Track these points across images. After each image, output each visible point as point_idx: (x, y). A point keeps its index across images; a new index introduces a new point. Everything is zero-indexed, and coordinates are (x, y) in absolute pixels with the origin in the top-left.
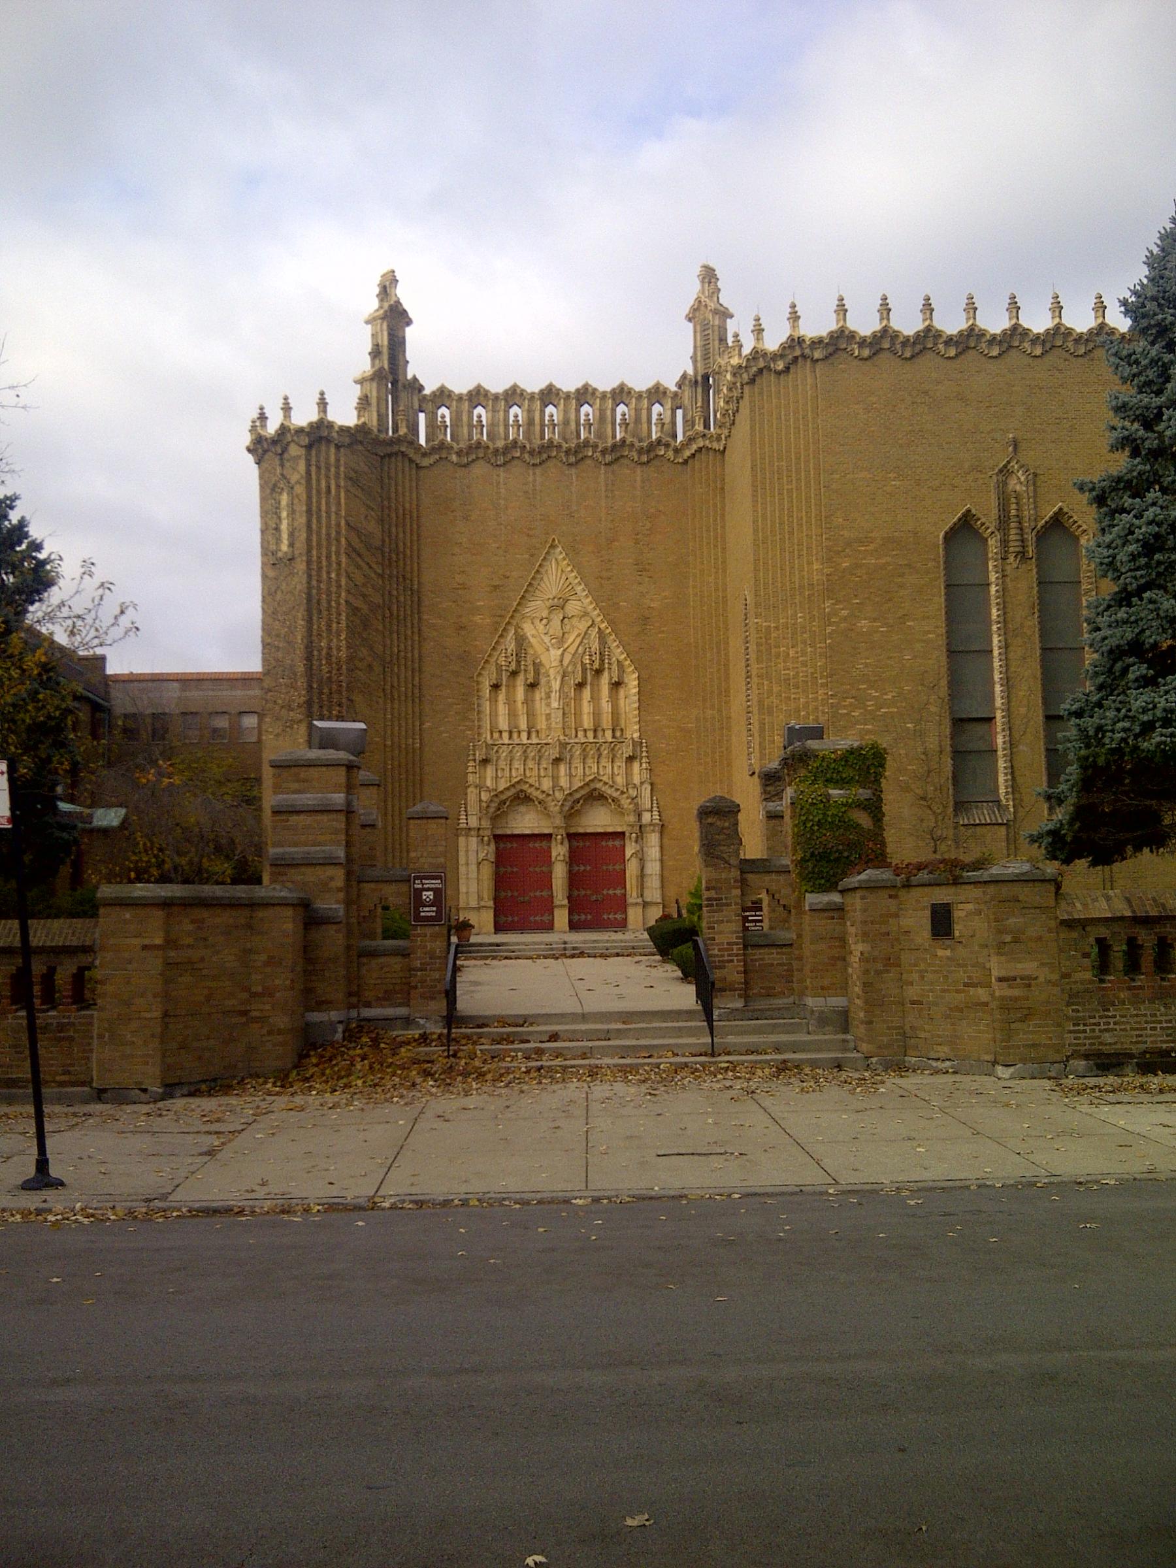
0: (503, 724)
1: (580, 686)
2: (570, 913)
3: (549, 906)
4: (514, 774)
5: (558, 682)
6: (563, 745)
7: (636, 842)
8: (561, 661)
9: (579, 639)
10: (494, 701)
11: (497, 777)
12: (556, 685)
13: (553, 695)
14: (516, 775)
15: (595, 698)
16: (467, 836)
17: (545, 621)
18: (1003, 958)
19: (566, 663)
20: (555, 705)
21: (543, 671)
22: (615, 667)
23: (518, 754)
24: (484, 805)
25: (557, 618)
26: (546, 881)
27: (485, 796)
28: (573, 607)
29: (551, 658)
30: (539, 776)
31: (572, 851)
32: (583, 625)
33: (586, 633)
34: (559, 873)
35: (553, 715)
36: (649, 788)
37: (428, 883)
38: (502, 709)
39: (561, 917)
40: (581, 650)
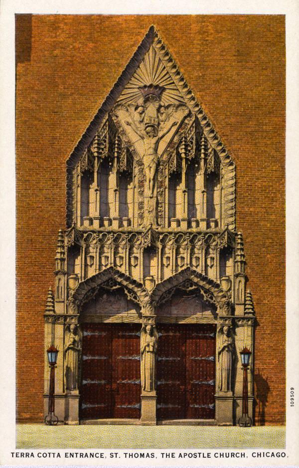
0: (94, 211)
1: (175, 178)
2: (157, 403)
3: (135, 394)
4: (103, 263)
5: (153, 171)
6: (155, 236)
7: (228, 336)
8: (156, 150)
9: (174, 129)
10: (86, 187)
11: (162, 265)
12: (150, 174)
13: (146, 184)
14: (107, 264)
15: (190, 189)
16: (54, 323)
17: (140, 109)
18: (172, 305)
19: (160, 152)
20: (148, 192)
21: (136, 159)
22: (211, 159)
23: (109, 242)
24: (72, 292)
25: (151, 109)
26: (134, 370)
27: (73, 284)
28: (168, 98)
29: (143, 148)
30: (206, 266)
31: (160, 341)
32: (179, 116)
33: (183, 122)
34: (147, 363)
35: (146, 202)
36: (243, 280)
37: (150, 95)
38: (93, 196)
39: (149, 407)
40: (176, 139)
